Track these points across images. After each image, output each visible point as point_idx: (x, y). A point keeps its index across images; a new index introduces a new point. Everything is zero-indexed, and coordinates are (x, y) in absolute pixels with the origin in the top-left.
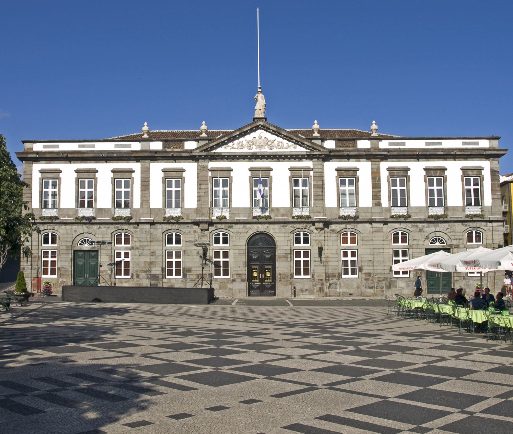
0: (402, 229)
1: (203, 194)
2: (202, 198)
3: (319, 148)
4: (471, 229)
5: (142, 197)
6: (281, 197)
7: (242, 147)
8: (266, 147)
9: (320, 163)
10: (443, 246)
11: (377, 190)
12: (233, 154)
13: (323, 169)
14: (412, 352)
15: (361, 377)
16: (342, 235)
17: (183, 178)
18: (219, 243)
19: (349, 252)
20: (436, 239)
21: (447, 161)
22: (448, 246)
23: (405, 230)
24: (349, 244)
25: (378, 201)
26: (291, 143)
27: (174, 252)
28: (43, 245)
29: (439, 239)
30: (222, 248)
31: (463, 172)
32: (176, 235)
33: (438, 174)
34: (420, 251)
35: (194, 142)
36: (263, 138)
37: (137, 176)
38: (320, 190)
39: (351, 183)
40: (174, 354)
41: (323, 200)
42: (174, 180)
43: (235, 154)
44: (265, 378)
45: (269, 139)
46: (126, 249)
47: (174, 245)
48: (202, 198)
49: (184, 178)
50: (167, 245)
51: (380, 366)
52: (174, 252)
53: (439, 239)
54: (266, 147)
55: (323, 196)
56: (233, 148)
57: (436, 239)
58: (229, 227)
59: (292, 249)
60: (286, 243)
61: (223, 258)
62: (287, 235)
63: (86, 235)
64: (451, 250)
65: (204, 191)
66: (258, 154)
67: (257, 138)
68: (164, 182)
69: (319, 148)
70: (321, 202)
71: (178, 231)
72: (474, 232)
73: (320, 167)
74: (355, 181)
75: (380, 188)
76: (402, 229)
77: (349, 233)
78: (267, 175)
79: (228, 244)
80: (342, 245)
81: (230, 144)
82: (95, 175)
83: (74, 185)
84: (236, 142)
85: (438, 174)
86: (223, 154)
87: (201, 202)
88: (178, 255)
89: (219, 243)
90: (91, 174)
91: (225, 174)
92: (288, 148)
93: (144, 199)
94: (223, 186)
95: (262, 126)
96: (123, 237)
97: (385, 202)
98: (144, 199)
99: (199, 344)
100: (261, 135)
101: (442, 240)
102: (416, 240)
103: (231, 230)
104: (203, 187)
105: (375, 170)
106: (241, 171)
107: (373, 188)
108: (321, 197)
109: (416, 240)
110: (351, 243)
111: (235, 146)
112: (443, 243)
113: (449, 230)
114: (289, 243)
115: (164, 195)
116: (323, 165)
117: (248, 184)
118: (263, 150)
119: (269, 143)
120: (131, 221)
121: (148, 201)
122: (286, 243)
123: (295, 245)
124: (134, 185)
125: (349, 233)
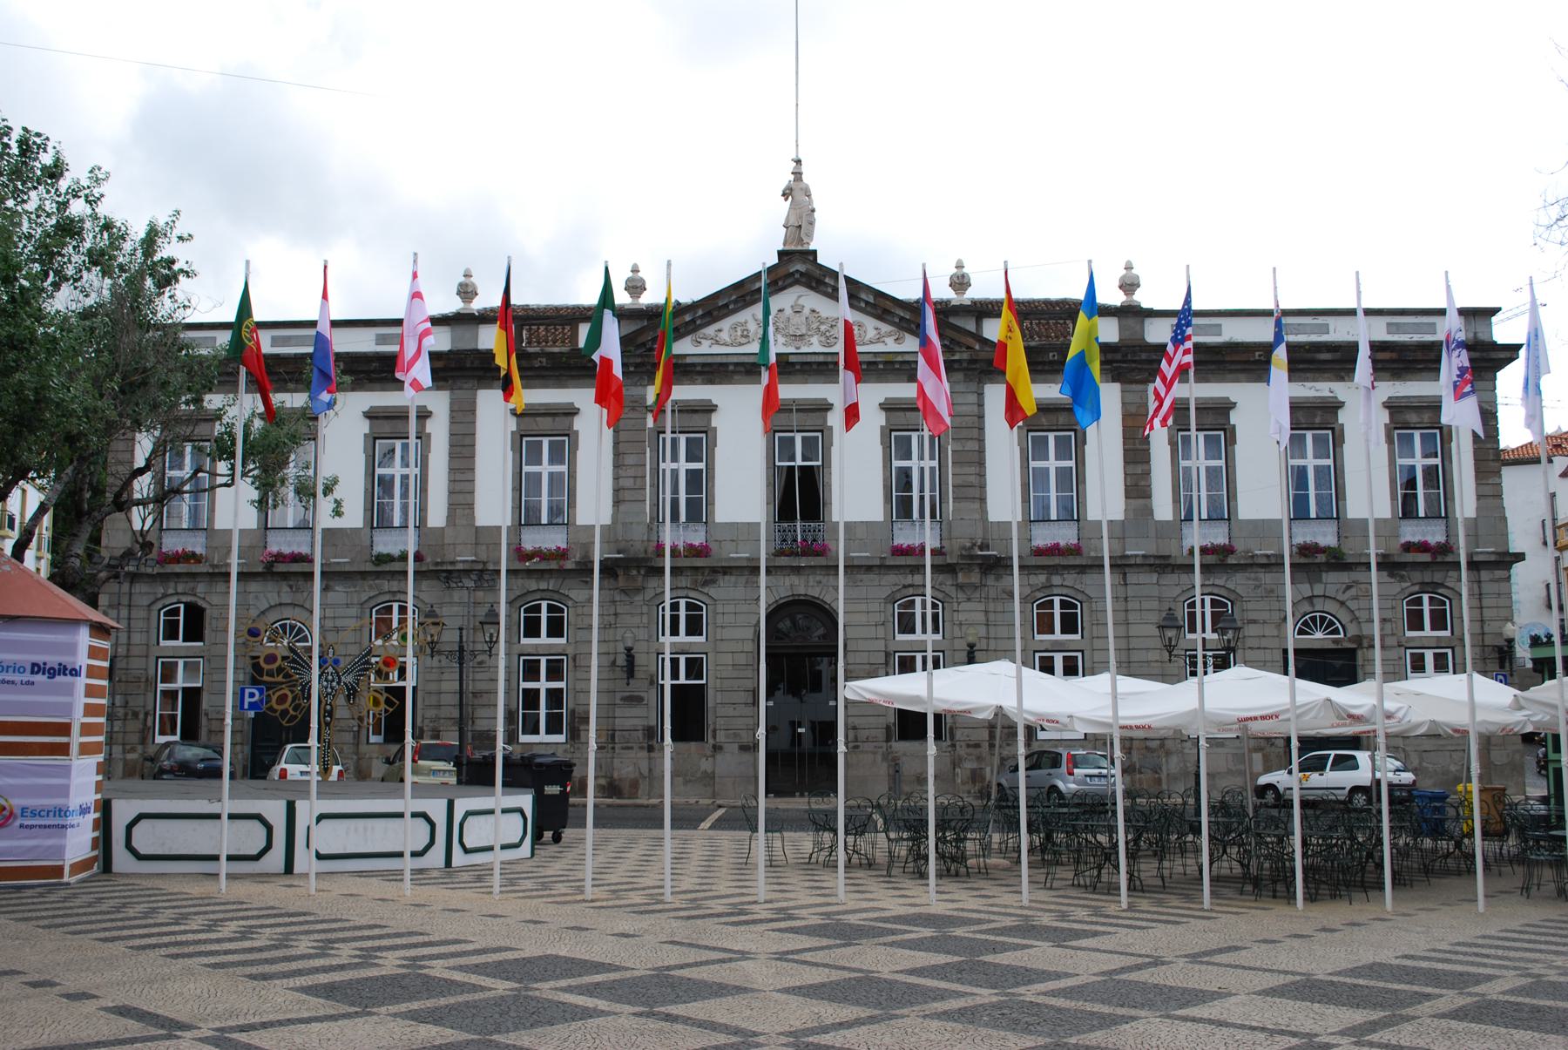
0: (1065, 591)
1: (628, 483)
2: (627, 495)
3: (970, 341)
4: (1417, 588)
5: (451, 493)
6: (856, 491)
7: (743, 340)
8: (815, 340)
9: (973, 386)
10: (1335, 641)
11: (1139, 469)
12: (718, 360)
13: (981, 405)
14: (1084, 943)
15: (898, 1012)
16: (526, 611)
17: (710, 433)
18: (539, 636)
19: (1429, 656)
20: (1313, 619)
21: (1207, 381)
22: (1350, 640)
23: (1223, 592)
24: (1428, 631)
25: (1141, 501)
26: (885, 328)
27: (543, 661)
28: (163, 643)
29: (1323, 619)
30: (686, 649)
31: (1391, 415)
32: (551, 609)
33: (1318, 420)
34: (1269, 658)
35: (1145, 305)
36: (806, 311)
37: (439, 429)
38: (972, 470)
39: (556, 458)
40: (849, 950)
41: (983, 500)
42: (546, 441)
43: (724, 360)
44: (640, 1015)
45: (824, 314)
46: (1438, 644)
47: (544, 639)
48: (627, 495)
49: (429, 435)
50: (524, 641)
51: (909, 986)
52: (543, 661)
53: (1323, 619)
54: (815, 340)
55: (983, 487)
56: (717, 343)
57: (1313, 619)
58: (705, 583)
59: (892, 648)
60: (871, 632)
61: (548, 679)
62: (875, 607)
63: (287, 612)
64: (1359, 653)
65: (631, 472)
66: (792, 359)
67: (788, 311)
68: (517, 447)
69: (970, 341)
70: (977, 505)
71: (556, 596)
72: (1426, 598)
73: (973, 398)
74: (565, 448)
75: (1148, 461)
76: (1216, 591)
77: (1057, 600)
78: (819, 422)
79: (701, 634)
80: (1038, 637)
81: (710, 330)
82: (571, 425)
83: (880, 448)
84: (726, 324)
85: (1318, 420)
86: (689, 360)
87: (622, 508)
88: (555, 672)
89: (539, 636)
90: (560, 423)
91: (811, 420)
92: (879, 340)
93: (460, 498)
94: (552, 461)
95: (802, 274)
96: (544, 615)
97: (1163, 508)
98: (460, 498)
99: (889, 926)
100: (801, 302)
101: (1331, 623)
102: (1255, 622)
103: (712, 591)
104: (629, 460)
105: (1133, 409)
106: (738, 415)
107: (1126, 462)
108: (974, 491)
109: (1255, 622)
110: (1433, 629)
111: (725, 336)
112: (1336, 631)
113: (1353, 592)
114: (881, 632)
115: (517, 489)
116: (981, 395)
117: (878, 450)
118: (804, 350)
119: (823, 328)
120: (1231, 560)
121: (471, 506)
122: (871, 632)
123: (900, 637)
124: (431, 456)
125: (1057, 600)
